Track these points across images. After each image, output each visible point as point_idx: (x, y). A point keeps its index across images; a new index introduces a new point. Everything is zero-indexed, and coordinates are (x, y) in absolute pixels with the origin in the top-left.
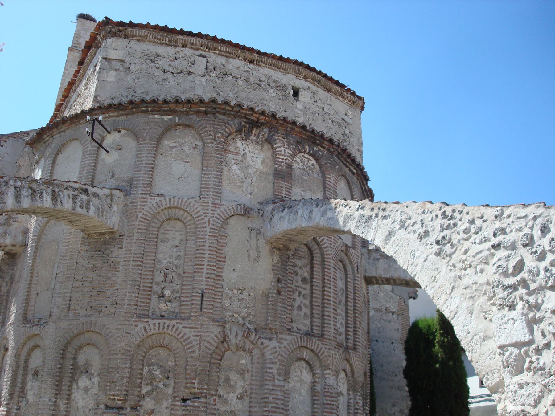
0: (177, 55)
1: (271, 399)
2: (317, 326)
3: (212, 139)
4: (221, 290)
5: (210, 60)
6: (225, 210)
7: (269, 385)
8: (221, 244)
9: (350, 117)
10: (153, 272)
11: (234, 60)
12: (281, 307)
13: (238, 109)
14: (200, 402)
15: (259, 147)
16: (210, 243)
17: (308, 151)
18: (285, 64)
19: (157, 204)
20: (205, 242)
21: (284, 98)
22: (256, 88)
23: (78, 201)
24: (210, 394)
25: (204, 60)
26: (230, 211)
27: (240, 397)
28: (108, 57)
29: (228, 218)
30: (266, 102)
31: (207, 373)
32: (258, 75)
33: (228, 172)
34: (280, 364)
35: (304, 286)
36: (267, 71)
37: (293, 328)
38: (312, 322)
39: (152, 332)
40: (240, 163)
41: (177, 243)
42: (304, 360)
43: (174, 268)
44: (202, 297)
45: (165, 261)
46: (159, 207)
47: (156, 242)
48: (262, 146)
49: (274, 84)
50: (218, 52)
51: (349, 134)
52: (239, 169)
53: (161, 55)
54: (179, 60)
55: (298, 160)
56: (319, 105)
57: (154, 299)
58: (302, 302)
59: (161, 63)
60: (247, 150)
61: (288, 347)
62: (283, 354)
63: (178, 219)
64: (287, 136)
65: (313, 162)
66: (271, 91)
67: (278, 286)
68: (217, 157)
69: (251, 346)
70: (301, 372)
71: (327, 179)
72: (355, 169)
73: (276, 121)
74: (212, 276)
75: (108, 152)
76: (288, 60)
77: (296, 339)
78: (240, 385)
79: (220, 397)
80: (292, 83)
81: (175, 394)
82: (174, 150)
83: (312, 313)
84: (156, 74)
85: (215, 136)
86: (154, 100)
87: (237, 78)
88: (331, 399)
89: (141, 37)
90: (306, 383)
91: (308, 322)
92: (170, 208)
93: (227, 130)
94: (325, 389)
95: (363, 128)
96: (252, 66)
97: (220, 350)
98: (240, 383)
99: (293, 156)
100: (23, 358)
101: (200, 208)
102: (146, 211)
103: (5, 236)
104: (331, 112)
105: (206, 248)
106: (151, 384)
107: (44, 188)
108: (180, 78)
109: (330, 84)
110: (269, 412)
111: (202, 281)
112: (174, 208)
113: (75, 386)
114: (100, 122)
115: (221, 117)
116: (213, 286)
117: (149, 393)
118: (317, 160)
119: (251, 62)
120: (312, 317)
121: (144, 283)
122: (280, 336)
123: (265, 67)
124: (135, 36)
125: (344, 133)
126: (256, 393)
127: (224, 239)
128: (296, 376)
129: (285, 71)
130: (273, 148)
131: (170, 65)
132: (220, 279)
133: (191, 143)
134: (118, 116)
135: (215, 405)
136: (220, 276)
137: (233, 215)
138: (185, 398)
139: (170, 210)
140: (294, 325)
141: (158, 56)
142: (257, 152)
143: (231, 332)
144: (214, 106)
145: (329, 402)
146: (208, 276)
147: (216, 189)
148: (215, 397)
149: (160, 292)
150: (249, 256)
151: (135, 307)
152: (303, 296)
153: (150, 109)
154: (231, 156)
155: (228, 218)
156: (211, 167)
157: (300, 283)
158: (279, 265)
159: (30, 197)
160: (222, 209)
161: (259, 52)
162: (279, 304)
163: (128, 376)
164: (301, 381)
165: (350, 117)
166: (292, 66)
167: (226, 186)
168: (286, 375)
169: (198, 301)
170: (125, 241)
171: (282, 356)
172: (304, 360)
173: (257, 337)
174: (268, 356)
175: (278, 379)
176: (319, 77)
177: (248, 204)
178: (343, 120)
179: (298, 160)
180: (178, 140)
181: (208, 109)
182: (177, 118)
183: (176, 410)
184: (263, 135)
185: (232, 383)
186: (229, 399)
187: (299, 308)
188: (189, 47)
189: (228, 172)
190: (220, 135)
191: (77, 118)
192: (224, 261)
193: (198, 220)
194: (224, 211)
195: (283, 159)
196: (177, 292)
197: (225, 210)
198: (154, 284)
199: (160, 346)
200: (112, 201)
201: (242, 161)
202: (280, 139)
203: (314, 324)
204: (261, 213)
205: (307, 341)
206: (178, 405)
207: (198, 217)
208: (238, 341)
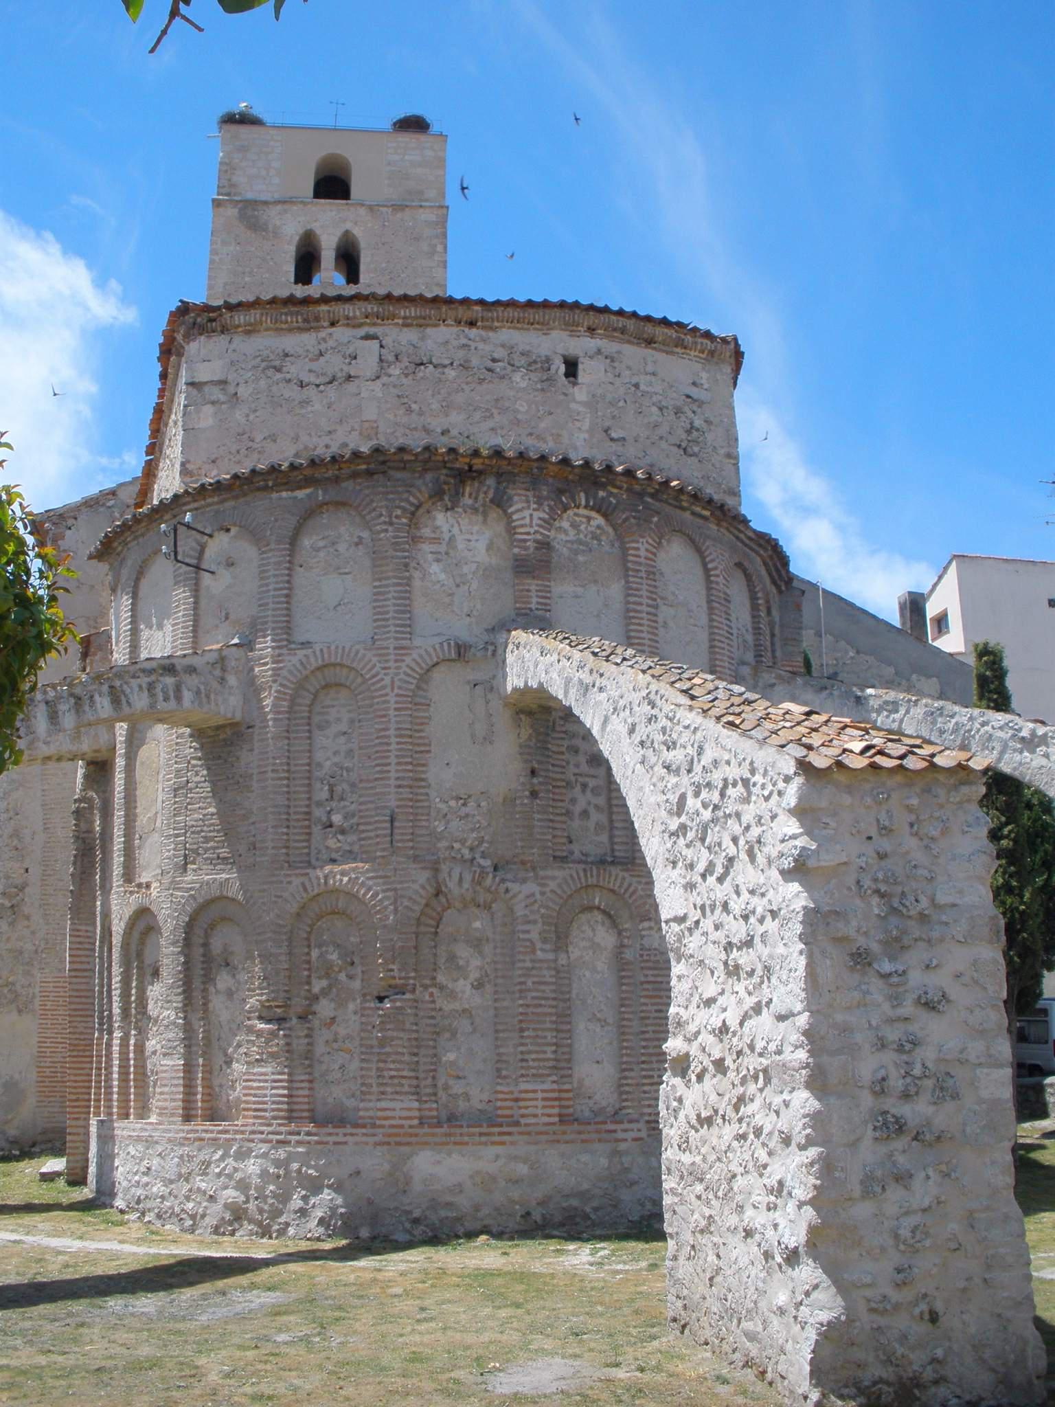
0: (323, 347)
1: (529, 984)
2: (623, 843)
3: (385, 523)
4: (426, 804)
5: (387, 341)
6: (421, 656)
7: (524, 961)
8: (418, 721)
9: (706, 386)
10: (309, 785)
11: (434, 329)
12: (539, 820)
13: (427, 455)
14: (405, 1000)
15: (480, 518)
16: (397, 722)
17: (583, 502)
18: (541, 312)
19: (302, 663)
20: (389, 721)
21: (545, 385)
22: (484, 379)
23: (158, 690)
24: (422, 986)
25: (375, 344)
26: (430, 655)
27: (478, 986)
28: (197, 380)
29: (428, 670)
30: (507, 404)
31: (414, 951)
32: (488, 348)
33: (422, 579)
34: (544, 923)
35: (592, 771)
36: (507, 335)
37: (572, 853)
38: (611, 837)
39: (316, 892)
40: (445, 557)
41: (343, 727)
42: (598, 908)
43: (345, 774)
44: (392, 821)
45: (328, 763)
46: (305, 668)
47: (309, 731)
48: (485, 514)
49: (523, 361)
50: (400, 321)
51: (705, 426)
52: (444, 571)
53: (292, 352)
54: (327, 356)
55: (565, 524)
56: (627, 380)
57: (316, 829)
58: (589, 803)
59: (294, 369)
60: (456, 530)
61: (559, 892)
62: (551, 904)
63: (341, 685)
64: (535, 483)
65: (599, 520)
66: (517, 377)
67: (532, 784)
68: (397, 557)
69: (489, 897)
70: (593, 930)
71: (631, 552)
72: (704, 508)
73: (505, 462)
74: (405, 783)
75: (212, 573)
76: (546, 304)
77: (575, 875)
78: (474, 964)
79: (442, 988)
80: (560, 350)
81: (365, 991)
82: (322, 554)
83: (611, 821)
84: (287, 394)
85: (390, 516)
86: (273, 467)
87: (445, 366)
88: (656, 972)
89: (250, 325)
90: (606, 949)
91: (604, 838)
92: (325, 666)
93: (411, 499)
94: (642, 956)
95: (736, 404)
96: (473, 332)
97: (434, 910)
98: (476, 962)
99: (548, 523)
100: (133, 947)
101: (375, 659)
102: (285, 678)
103: (79, 737)
104: (658, 388)
105: (392, 732)
106: (327, 976)
107: (94, 687)
108: (331, 391)
109: (649, 329)
110: (528, 1006)
111: (389, 793)
112: (334, 665)
113: (212, 989)
114: (188, 526)
115: (398, 475)
116: (411, 800)
117: (325, 992)
118: (605, 516)
119: (472, 324)
120: (612, 828)
121: (295, 806)
122: (542, 873)
123: (501, 327)
124: (239, 326)
125: (692, 428)
126: (503, 977)
127: (424, 711)
128: (583, 939)
129: (545, 327)
130: (509, 516)
131: (310, 371)
132: (423, 784)
133: (351, 535)
134: (222, 502)
135: (433, 1002)
136: (423, 780)
137: (437, 664)
138: (382, 994)
139: (326, 670)
140: (576, 848)
141: (287, 355)
142: (476, 528)
143: (450, 876)
144: (381, 458)
145: (652, 979)
146: (399, 782)
147: (400, 619)
148: (431, 990)
149: (324, 819)
150: (473, 736)
151: (284, 851)
152: (592, 791)
153: (270, 483)
154: (426, 547)
155: (428, 670)
156: (388, 578)
157: (585, 768)
158: (532, 744)
159: (73, 711)
160: (415, 656)
161: (481, 302)
162: (537, 816)
163: (286, 966)
164: (595, 947)
165: (706, 386)
166: (557, 313)
167: (421, 608)
168: (560, 940)
169: (385, 829)
170: (256, 738)
171: (547, 908)
172: (598, 908)
173: (497, 879)
174: (520, 911)
175: (542, 950)
176: (620, 322)
177: (465, 636)
178: (688, 396)
179: (565, 524)
180: (326, 534)
181: (372, 466)
182: (320, 492)
183: (368, 1016)
184: (485, 493)
185: (461, 963)
186: (458, 990)
187: (585, 814)
188: (344, 325)
189: (422, 579)
190: (399, 512)
191: (163, 507)
192: (429, 752)
193: (373, 684)
194: (419, 660)
195: (528, 533)
196: (353, 815)
197: (421, 656)
198: (313, 806)
199: (333, 913)
200: (224, 670)
201: (447, 553)
202: (520, 495)
203: (616, 840)
204: (491, 648)
205: (598, 875)
206: (370, 1008)
207: (374, 676)
208: (463, 891)
